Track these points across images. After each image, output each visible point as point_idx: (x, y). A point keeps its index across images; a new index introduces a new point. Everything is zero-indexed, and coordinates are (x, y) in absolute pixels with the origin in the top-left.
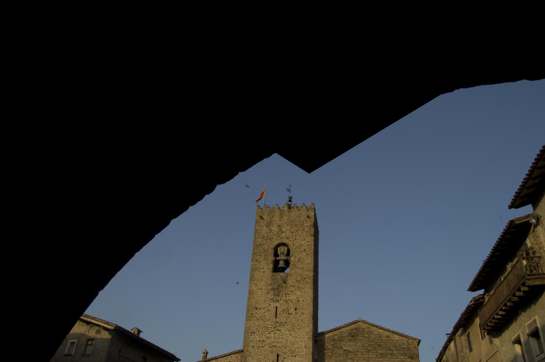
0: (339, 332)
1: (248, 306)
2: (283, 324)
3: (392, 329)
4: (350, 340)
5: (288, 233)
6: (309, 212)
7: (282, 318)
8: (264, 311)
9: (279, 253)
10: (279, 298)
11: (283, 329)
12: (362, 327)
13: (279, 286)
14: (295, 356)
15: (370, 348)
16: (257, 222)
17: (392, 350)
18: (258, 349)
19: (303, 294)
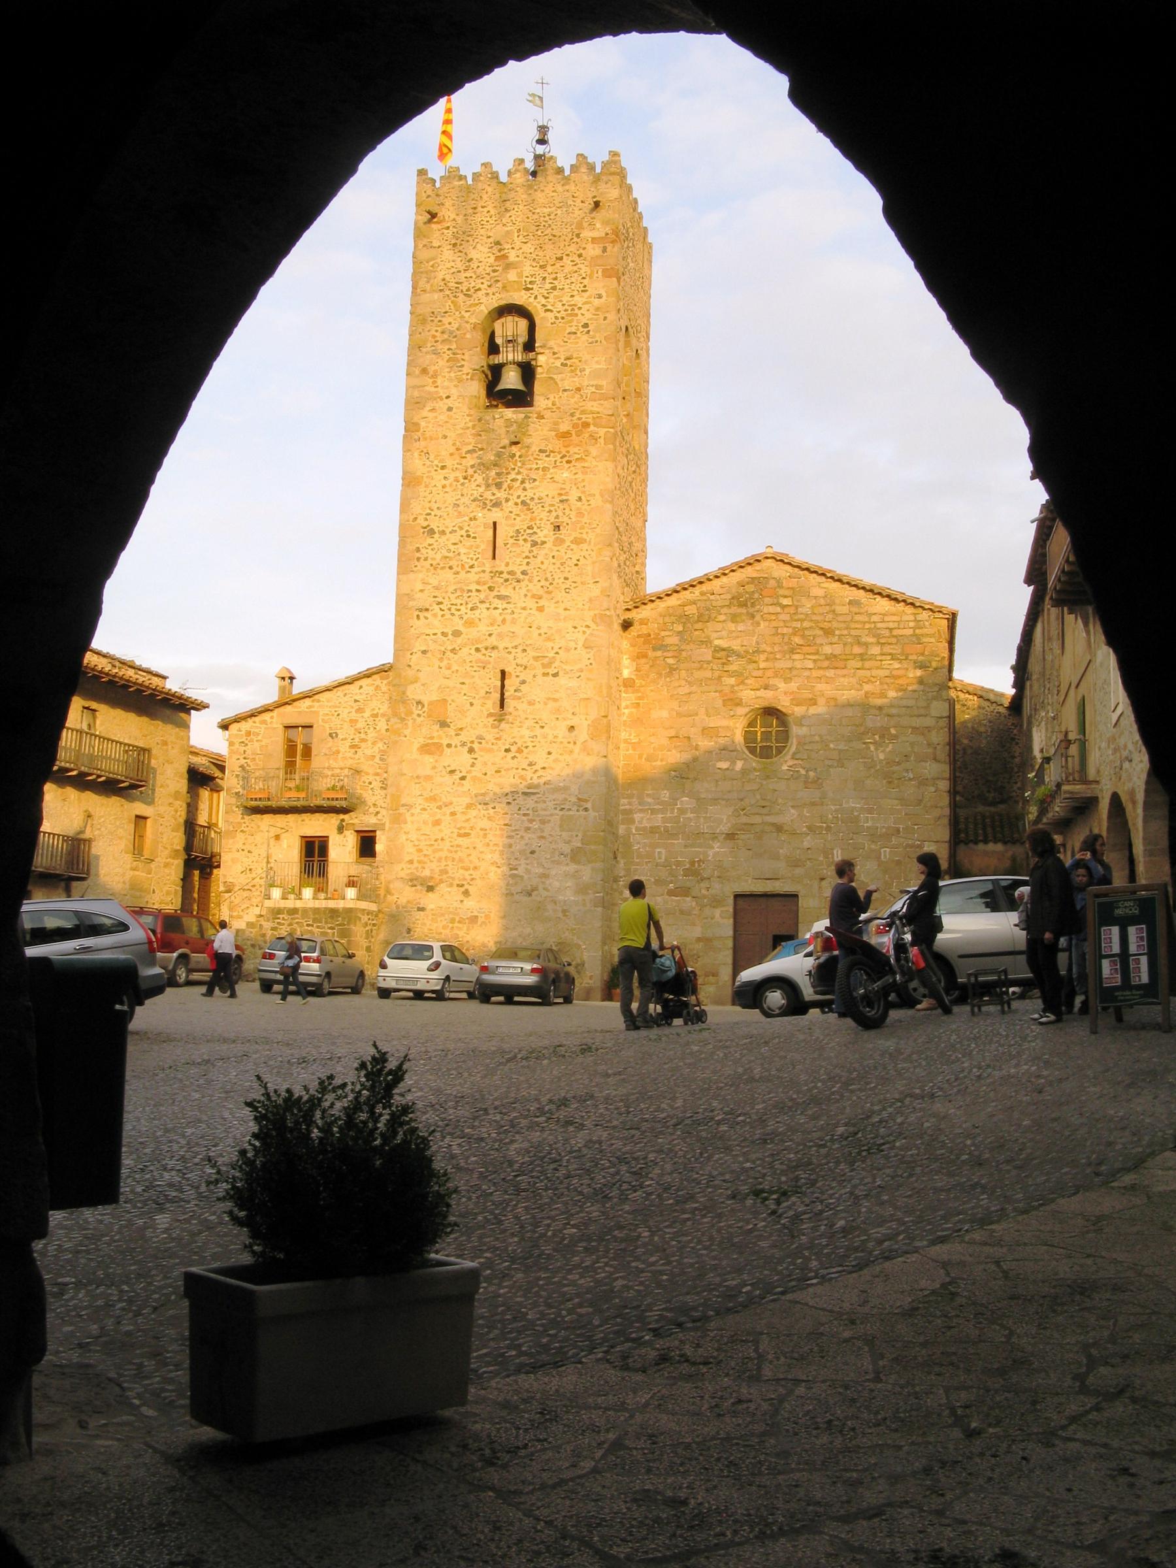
0: (702, 594)
1: (403, 527)
2: (513, 578)
3: (868, 580)
4: (734, 618)
5: (527, 270)
6: (602, 187)
7: (512, 558)
8: (454, 538)
9: (499, 341)
10: (501, 495)
11: (518, 595)
12: (776, 574)
13: (499, 455)
14: (555, 675)
15: (797, 640)
16: (419, 234)
17: (866, 645)
18: (441, 660)
19: (580, 476)
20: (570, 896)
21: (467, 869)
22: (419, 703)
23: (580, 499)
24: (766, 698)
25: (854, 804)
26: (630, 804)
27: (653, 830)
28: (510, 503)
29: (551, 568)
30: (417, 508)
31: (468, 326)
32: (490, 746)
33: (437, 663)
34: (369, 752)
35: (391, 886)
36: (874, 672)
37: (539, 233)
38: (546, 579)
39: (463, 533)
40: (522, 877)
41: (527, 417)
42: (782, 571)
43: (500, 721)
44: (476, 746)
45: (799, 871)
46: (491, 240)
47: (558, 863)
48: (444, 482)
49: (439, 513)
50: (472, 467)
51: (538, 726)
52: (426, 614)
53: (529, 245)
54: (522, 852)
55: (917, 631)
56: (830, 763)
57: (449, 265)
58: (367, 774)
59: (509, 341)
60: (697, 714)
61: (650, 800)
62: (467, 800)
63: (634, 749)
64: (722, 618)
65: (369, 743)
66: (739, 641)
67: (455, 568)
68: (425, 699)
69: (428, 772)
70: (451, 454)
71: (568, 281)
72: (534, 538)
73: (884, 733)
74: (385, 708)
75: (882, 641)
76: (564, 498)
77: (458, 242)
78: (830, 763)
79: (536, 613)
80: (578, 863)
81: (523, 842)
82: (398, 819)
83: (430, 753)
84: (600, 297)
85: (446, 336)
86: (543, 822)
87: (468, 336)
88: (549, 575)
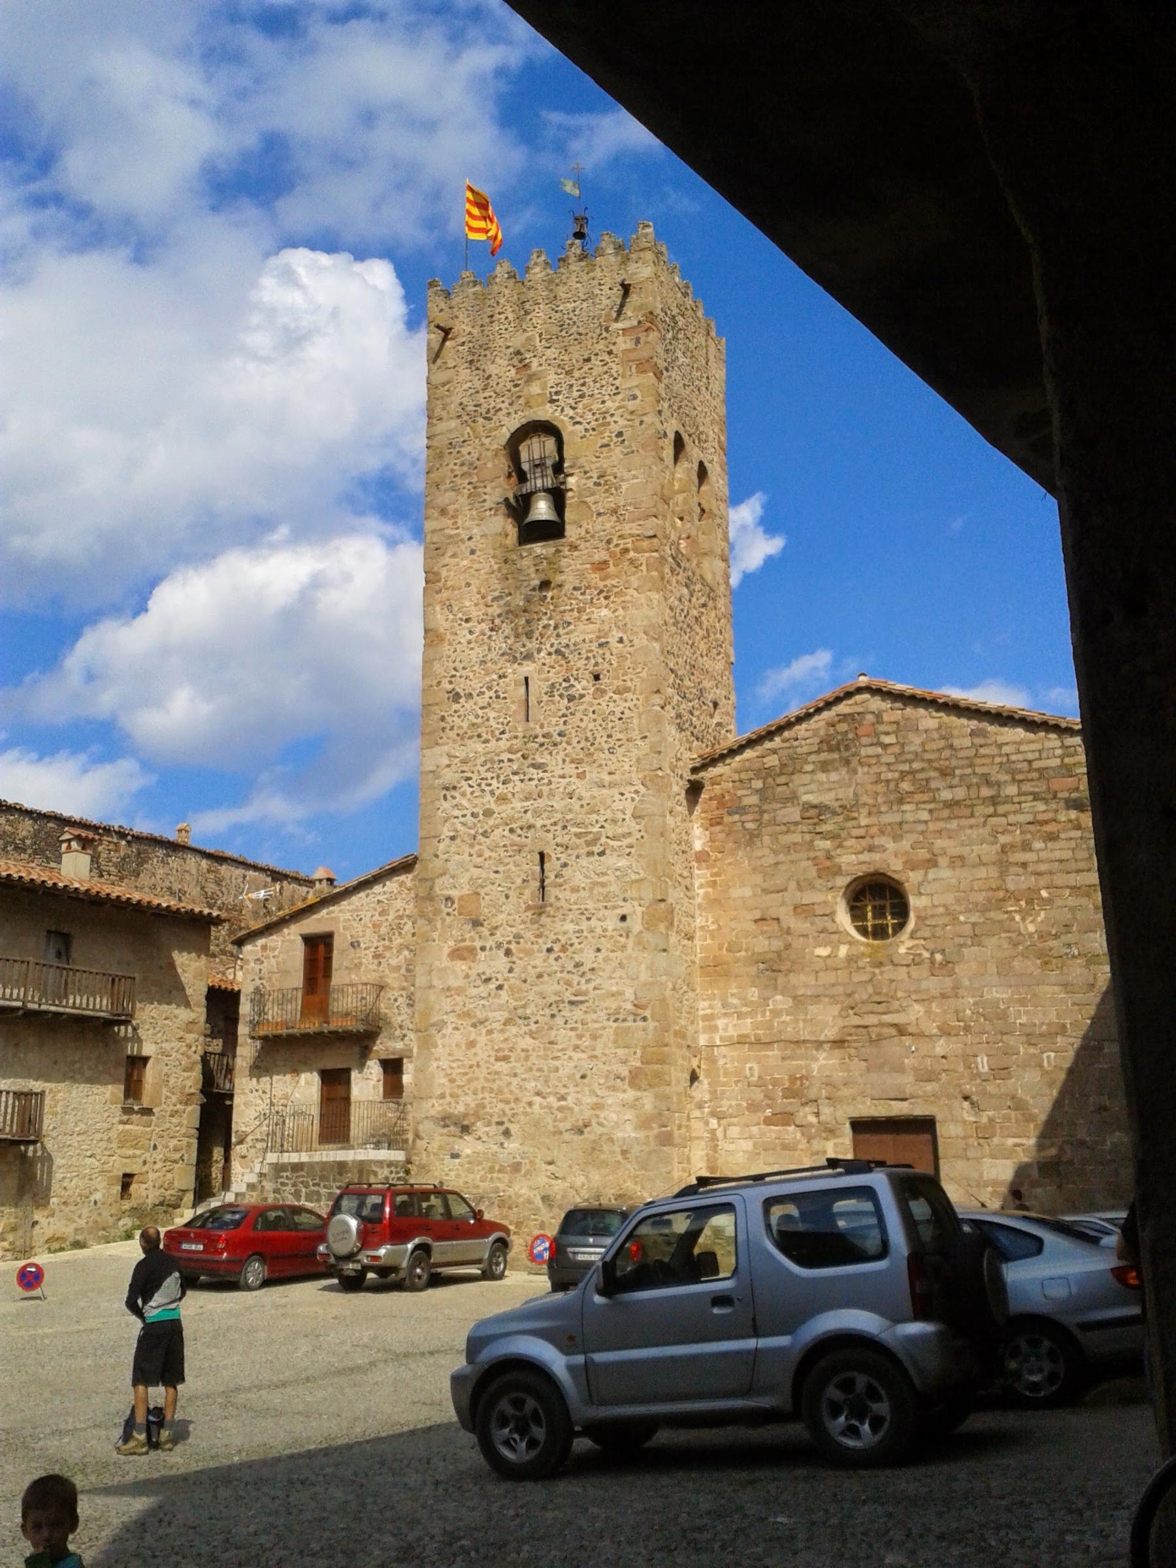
2: (549, 743)
4: (825, 767)
5: (552, 379)
8: (482, 701)
9: (525, 467)
10: (532, 645)
11: (554, 761)
13: (528, 600)
14: (601, 854)
17: (998, 784)
20: (628, 1132)
21: (508, 1102)
22: (448, 899)
23: (621, 641)
24: (873, 861)
25: (998, 993)
26: (711, 1007)
27: (741, 1041)
28: (542, 654)
29: (591, 726)
30: (437, 668)
31: (489, 454)
32: (529, 945)
33: (467, 849)
34: (394, 962)
35: (421, 1127)
36: (1012, 818)
37: (563, 333)
38: (587, 739)
39: (492, 693)
40: (571, 1109)
41: (558, 551)
42: (876, 703)
43: (540, 914)
44: (513, 947)
45: (929, 1087)
46: (511, 350)
47: (614, 1089)
48: (469, 637)
49: (464, 673)
50: (499, 616)
51: (584, 918)
52: (453, 793)
53: (553, 349)
54: (570, 1077)
55: (1067, 760)
56: (961, 940)
57: (466, 386)
58: (392, 989)
59: (537, 466)
60: (786, 890)
61: (735, 1001)
62: (506, 1015)
63: (713, 938)
64: (809, 768)
65: (394, 951)
66: (832, 795)
67: (485, 736)
68: (455, 893)
69: (460, 983)
70: (476, 605)
71: (598, 385)
72: (572, 692)
73: (1032, 898)
74: (410, 908)
75: (1020, 777)
76: (603, 640)
77: (475, 358)
78: (961, 940)
79: (577, 781)
80: (639, 1089)
81: (572, 1064)
82: (427, 1043)
83: (462, 958)
84: (635, 397)
85: (465, 469)
86: (594, 1037)
87: (489, 465)
88: (589, 734)
